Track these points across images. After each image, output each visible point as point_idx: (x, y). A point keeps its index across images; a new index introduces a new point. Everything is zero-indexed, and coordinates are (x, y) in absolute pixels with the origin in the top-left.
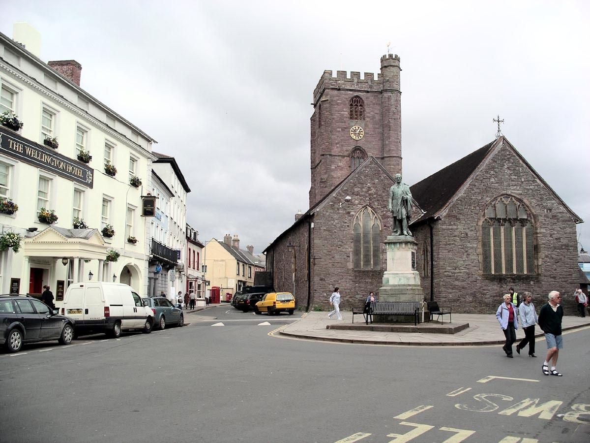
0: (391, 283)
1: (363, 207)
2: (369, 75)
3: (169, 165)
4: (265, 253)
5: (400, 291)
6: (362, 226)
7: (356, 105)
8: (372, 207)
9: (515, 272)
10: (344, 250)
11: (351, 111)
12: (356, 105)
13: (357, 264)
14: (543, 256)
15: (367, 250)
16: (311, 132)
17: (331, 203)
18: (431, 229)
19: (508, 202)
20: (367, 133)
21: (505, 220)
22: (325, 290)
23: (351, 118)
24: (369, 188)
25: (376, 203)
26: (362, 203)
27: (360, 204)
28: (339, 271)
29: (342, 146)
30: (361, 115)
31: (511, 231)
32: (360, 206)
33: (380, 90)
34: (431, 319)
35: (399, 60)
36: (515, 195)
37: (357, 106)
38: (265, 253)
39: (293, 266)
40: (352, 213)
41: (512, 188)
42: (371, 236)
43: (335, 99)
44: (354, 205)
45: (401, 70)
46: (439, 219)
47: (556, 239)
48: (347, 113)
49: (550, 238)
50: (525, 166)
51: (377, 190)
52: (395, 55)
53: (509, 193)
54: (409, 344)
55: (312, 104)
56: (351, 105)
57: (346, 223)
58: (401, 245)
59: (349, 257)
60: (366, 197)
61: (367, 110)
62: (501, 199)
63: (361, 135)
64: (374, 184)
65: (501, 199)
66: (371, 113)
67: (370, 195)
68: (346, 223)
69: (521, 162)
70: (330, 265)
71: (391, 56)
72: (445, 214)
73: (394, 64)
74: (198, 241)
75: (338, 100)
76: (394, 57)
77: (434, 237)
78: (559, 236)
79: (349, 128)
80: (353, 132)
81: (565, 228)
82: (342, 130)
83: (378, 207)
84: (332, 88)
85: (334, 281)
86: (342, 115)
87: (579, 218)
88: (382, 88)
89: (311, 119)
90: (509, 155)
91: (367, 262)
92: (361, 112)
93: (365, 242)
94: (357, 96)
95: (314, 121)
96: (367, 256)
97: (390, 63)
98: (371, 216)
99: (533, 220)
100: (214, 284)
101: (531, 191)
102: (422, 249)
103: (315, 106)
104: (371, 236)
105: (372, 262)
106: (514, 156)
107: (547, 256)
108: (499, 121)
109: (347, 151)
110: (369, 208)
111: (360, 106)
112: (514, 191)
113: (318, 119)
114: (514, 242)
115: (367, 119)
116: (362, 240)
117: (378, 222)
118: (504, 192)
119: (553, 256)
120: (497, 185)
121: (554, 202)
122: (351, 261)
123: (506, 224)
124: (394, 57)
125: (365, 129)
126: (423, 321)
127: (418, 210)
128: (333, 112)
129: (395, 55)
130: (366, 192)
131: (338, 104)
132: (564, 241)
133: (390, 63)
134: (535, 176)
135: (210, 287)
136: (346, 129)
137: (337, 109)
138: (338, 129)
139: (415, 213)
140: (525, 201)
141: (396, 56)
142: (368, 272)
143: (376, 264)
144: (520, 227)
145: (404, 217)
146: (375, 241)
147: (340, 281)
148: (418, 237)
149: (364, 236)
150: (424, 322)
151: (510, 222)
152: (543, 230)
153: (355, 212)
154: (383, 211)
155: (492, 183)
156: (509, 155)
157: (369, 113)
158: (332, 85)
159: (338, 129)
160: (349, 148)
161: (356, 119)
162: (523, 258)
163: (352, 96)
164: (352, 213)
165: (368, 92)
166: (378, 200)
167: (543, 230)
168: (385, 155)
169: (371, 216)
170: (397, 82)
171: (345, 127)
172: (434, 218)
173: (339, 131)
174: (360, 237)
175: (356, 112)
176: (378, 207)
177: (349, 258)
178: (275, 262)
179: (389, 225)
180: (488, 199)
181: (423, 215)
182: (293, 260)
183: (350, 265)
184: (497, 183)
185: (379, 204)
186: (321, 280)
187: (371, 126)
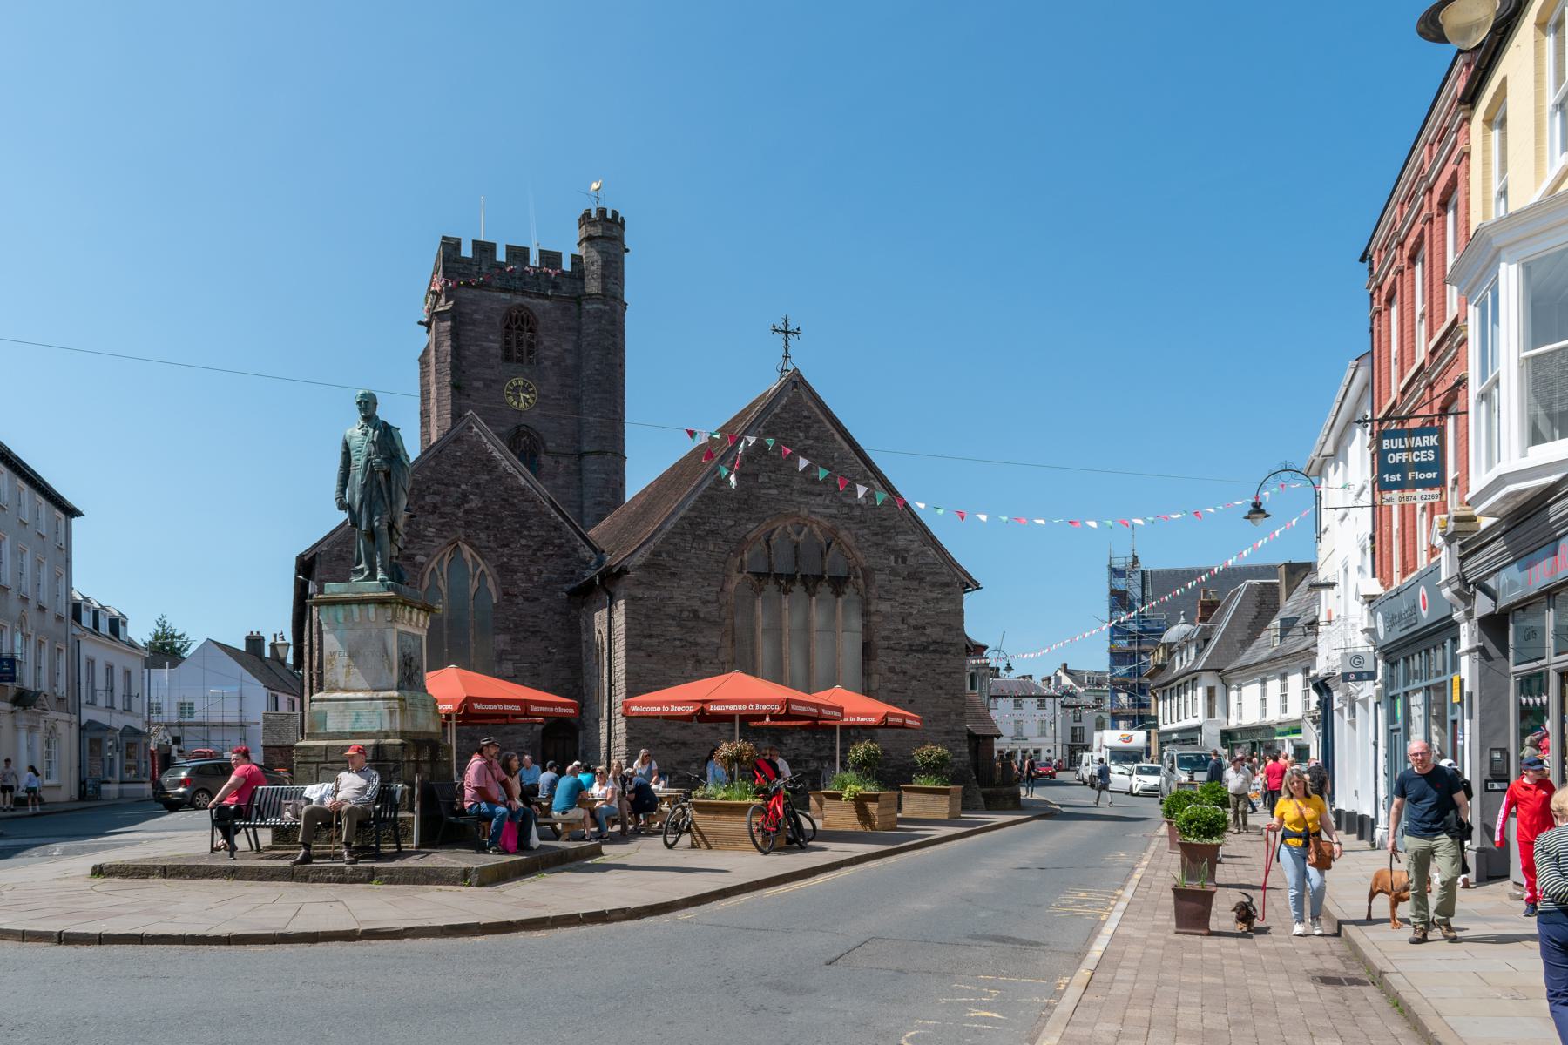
2: (550, 258)
6: (444, 591)
7: (519, 328)
8: (472, 546)
11: (508, 343)
14: (884, 667)
20: (545, 397)
21: (791, 578)
30: (530, 353)
47: (916, 628)
48: (497, 345)
54: (25, 936)
55: (420, 323)
56: (508, 327)
71: (603, 212)
75: (475, 312)
76: (609, 216)
81: (937, 600)
87: (970, 577)
97: (606, 231)
99: (861, 581)
103: (428, 325)
108: (786, 332)
115: (547, 363)
124: (609, 216)
132: (934, 633)
133: (606, 231)
152: (885, 607)
153: (427, 556)
155: (763, 486)
161: (520, 360)
166: (487, 528)
167: (885, 607)
168: (586, 449)
175: (519, 344)
179: (516, 590)
184: (777, 487)
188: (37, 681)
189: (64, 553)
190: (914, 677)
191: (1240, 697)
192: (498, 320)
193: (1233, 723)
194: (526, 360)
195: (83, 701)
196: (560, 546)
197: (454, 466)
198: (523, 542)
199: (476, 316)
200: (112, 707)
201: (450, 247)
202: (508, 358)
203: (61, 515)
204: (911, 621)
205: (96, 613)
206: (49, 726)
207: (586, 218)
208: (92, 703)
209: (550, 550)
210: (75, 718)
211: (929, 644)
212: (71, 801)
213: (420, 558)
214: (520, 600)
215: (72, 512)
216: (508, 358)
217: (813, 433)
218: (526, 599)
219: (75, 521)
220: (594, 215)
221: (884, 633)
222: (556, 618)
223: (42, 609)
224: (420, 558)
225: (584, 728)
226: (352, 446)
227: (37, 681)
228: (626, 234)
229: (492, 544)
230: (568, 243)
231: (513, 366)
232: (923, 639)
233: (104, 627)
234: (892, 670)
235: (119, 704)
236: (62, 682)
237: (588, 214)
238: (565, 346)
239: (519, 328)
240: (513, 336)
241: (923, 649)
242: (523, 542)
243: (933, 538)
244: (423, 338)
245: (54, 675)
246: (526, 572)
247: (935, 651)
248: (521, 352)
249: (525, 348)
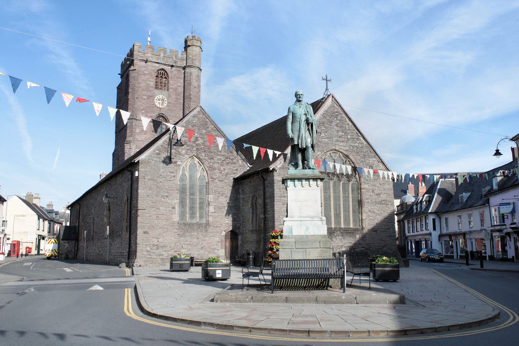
0: (295, 233)
4: (70, 208)
5: (303, 241)
7: (162, 78)
9: (342, 226)
10: (170, 201)
11: (156, 82)
13: (182, 215)
14: (367, 210)
15: (193, 201)
17: (157, 152)
18: (264, 180)
19: (336, 158)
20: (170, 103)
22: (149, 243)
23: (156, 88)
25: (203, 154)
27: (186, 153)
30: (165, 86)
31: (339, 185)
32: (187, 156)
33: (183, 66)
36: (342, 151)
37: (162, 78)
38: (70, 208)
39: (106, 220)
41: (340, 144)
42: (197, 188)
43: (142, 69)
44: (181, 154)
46: (274, 170)
47: (377, 194)
48: (153, 83)
49: (372, 194)
50: (351, 124)
51: (204, 141)
53: (337, 148)
55: (119, 74)
56: (157, 76)
57: (172, 173)
59: (174, 208)
60: (193, 147)
61: (171, 82)
62: (330, 154)
65: (330, 154)
67: (197, 145)
69: (347, 120)
70: (155, 216)
72: (279, 166)
73: (196, 44)
75: (145, 70)
77: (267, 189)
78: (379, 192)
79: (153, 97)
82: (147, 98)
83: (206, 158)
85: (159, 234)
86: (149, 85)
88: (185, 65)
89: (118, 88)
90: (337, 112)
91: (338, 222)
92: (165, 83)
93: (192, 194)
95: (121, 90)
96: (192, 208)
100: (14, 238)
101: (356, 148)
102: (250, 203)
104: (197, 188)
105: (198, 215)
106: (341, 114)
107: (370, 211)
108: (327, 80)
110: (196, 159)
111: (165, 78)
112: (342, 148)
113: (124, 88)
114: (332, 199)
115: (171, 90)
116: (188, 191)
117: (205, 174)
118: (333, 147)
119: (375, 210)
120: (326, 140)
121: (375, 159)
122: (177, 213)
123: (334, 178)
125: (168, 99)
127: (244, 163)
128: (140, 81)
130: (194, 142)
131: (144, 74)
134: (359, 134)
135: (10, 242)
136: (151, 97)
137: (144, 79)
138: (144, 97)
139: (240, 166)
140: (351, 157)
142: (193, 224)
143: (201, 217)
144: (346, 182)
145: (310, 145)
146: (201, 192)
147: (164, 234)
148: (245, 190)
149: (190, 187)
151: (338, 177)
156: (337, 112)
157: (173, 85)
158: (140, 57)
159: (144, 97)
160: (153, 115)
161: (160, 89)
162: (349, 212)
165: (172, 66)
166: (205, 151)
172: (268, 169)
173: (145, 99)
174: (186, 188)
175: (161, 83)
176: (206, 158)
178: (81, 216)
179: (215, 177)
180: (319, 153)
181: (248, 168)
182: (106, 213)
183: (176, 218)
184: (327, 138)
185: (205, 154)
186: (145, 233)
187: (173, 97)
190: (377, 214)
191: (447, 223)
193: (444, 231)
196: (232, 159)
197: (193, 126)
198: (218, 157)
199: (145, 72)
204: (376, 192)
209: (228, 160)
211: (382, 201)
213: (179, 163)
217: (339, 118)
221: (367, 197)
224: (179, 163)
229: (206, 158)
232: (380, 199)
234: (370, 211)
238: (178, 84)
241: (381, 203)
242: (218, 157)
243: (77, 201)
246: (219, 170)
247: (384, 204)
249: (163, 85)
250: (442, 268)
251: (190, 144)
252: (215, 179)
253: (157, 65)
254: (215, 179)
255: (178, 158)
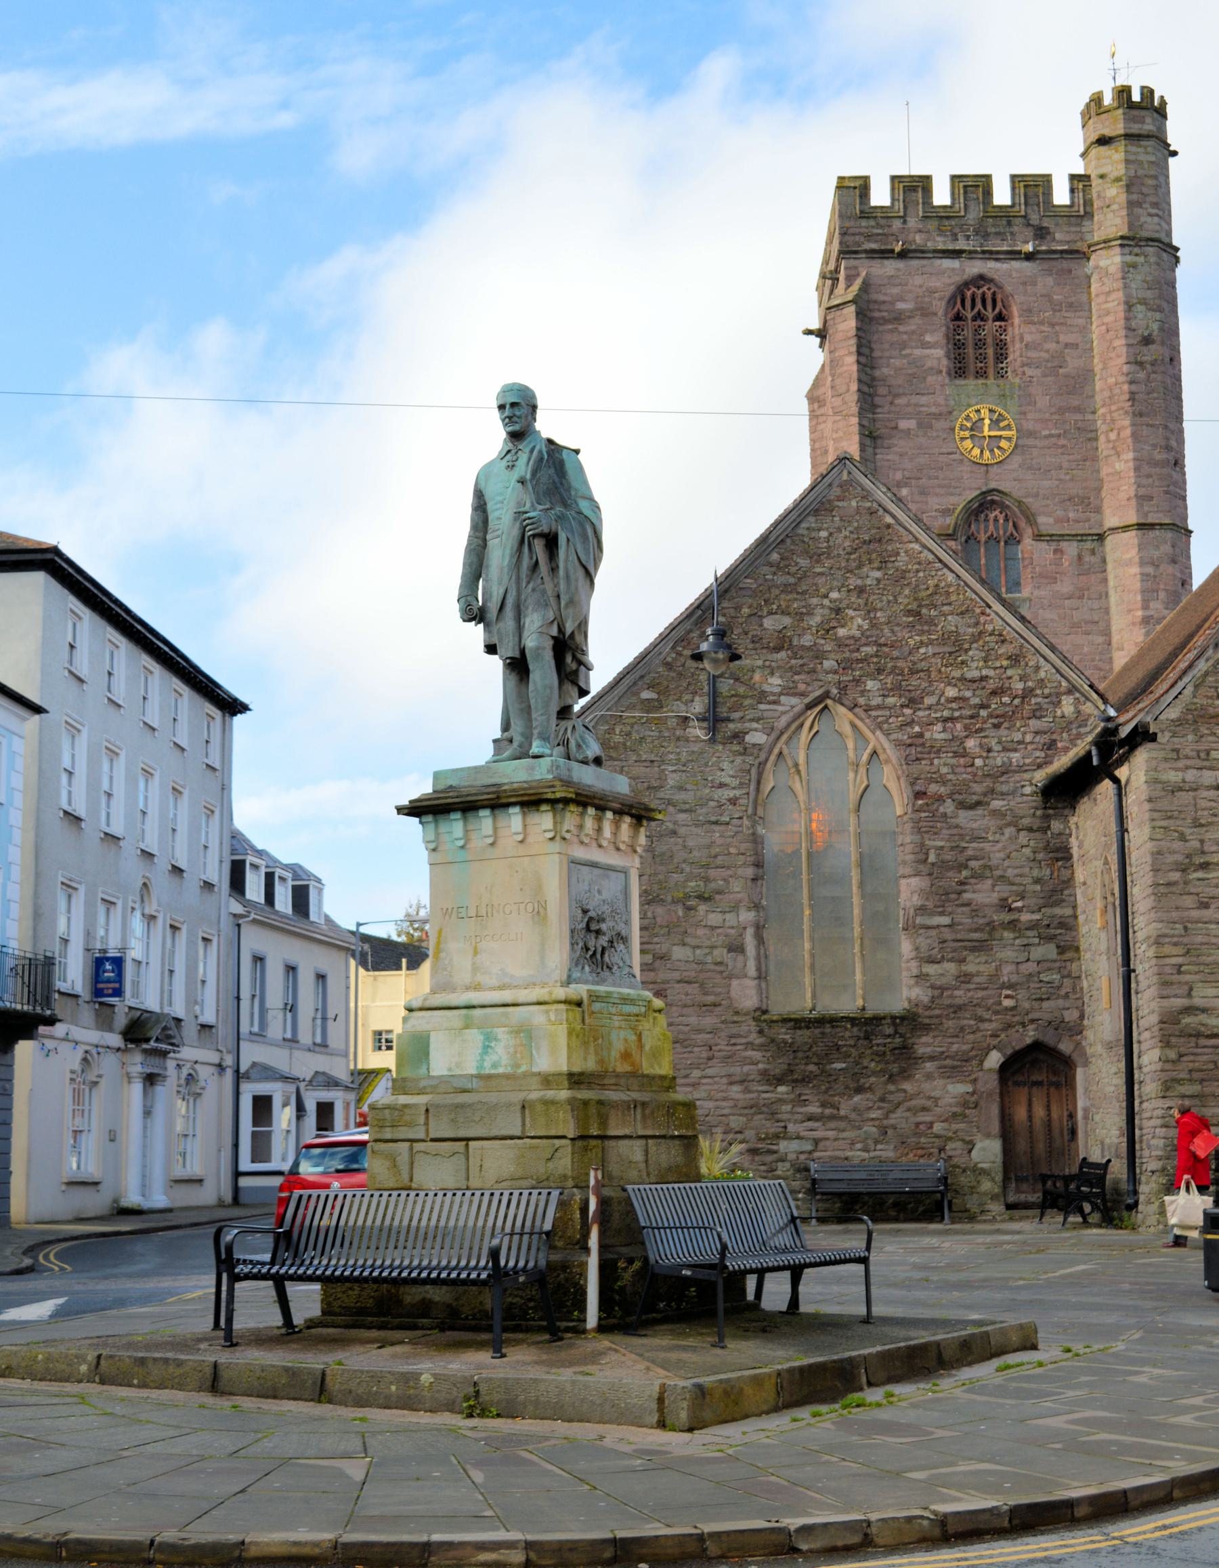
1: (809, 707)
2: (1033, 187)
3: (39, 578)
12: (979, 317)
16: (812, 450)
20: (1031, 434)
24: (838, 611)
26: (802, 687)
27: (789, 691)
28: (693, 1020)
29: (922, 493)
32: (794, 701)
34: (750, 1296)
35: (1161, 112)
40: (752, 738)
44: (762, 697)
45: (1174, 154)
48: (939, 353)
52: (1143, 88)
55: (809, 332)
56: (958, 317)
57: (722, 785)
58: (502, 822)
59: (737, 948)
63: (1004, 444)
64: (861, 590)
66: (1047, 346)
67: (841, 644)
68: (722, 785)
71: (1123, 92)
74: (328, 920)
76: (1136, 97)
80: (967, 434)
82: (920, 425)
84: (873, 251)
94: (981, 277)
97: (1135, 124)
98: (851, 745)
103: (822, 334)
109: (946, 512)
124: (1136, 97)
126: (592, 1317)
129: (1143, 88)
130: (827, 630)
133: (1135, 124)
141: (1148, 93)
147: (696, 1073)
150: (602, 1329)
154: (911, 723)
158: (869, 237)
161: (981, 374)
163: (958, 279)
164: (752, 738)
169: (851, 745)
170: (1155, 205)
171: (933, 410)
177: (740, 958)
188: (167, 994)
189: (218, 775)
192: (939, 306)
194: (991, 371)
195: (245, 1028)
198: (951, 692)
199: (901, 306)
200: (294, 1040)
201: (853, 190)
202: (959, 370)
203: (217, 713)
205: (270, 877)
206: (185, 1071)
207: (1095, 106)
208: (260, 1036)
210: (229, 1060)
212: (221, 1204)
214: (948, 807)
215: (232, 707)
216: (959, 370)
218: (963, 805)
219: (239, 719)
220: (1108, 100)
222: (1023, 837)
223: (177, 870)
225: (1086, 1064)
226: (488, 495)
227: (167, 994)
228: (1170, 124)
230: (1060, 156)
231: (971, 383)
233: (283, 901)
235: (305, 1037)
236: (210, 995)
237: (1097, 99)
239: (979, 317)
240: (968, 333)
244: (813, 356)
245: (195, 984)
248: (982, 358)
250: (1016, 1237)
251: (807, 640)
252: (940, 799)
253: (948, 263)
254: (940, 799)
255: (751, 714)
